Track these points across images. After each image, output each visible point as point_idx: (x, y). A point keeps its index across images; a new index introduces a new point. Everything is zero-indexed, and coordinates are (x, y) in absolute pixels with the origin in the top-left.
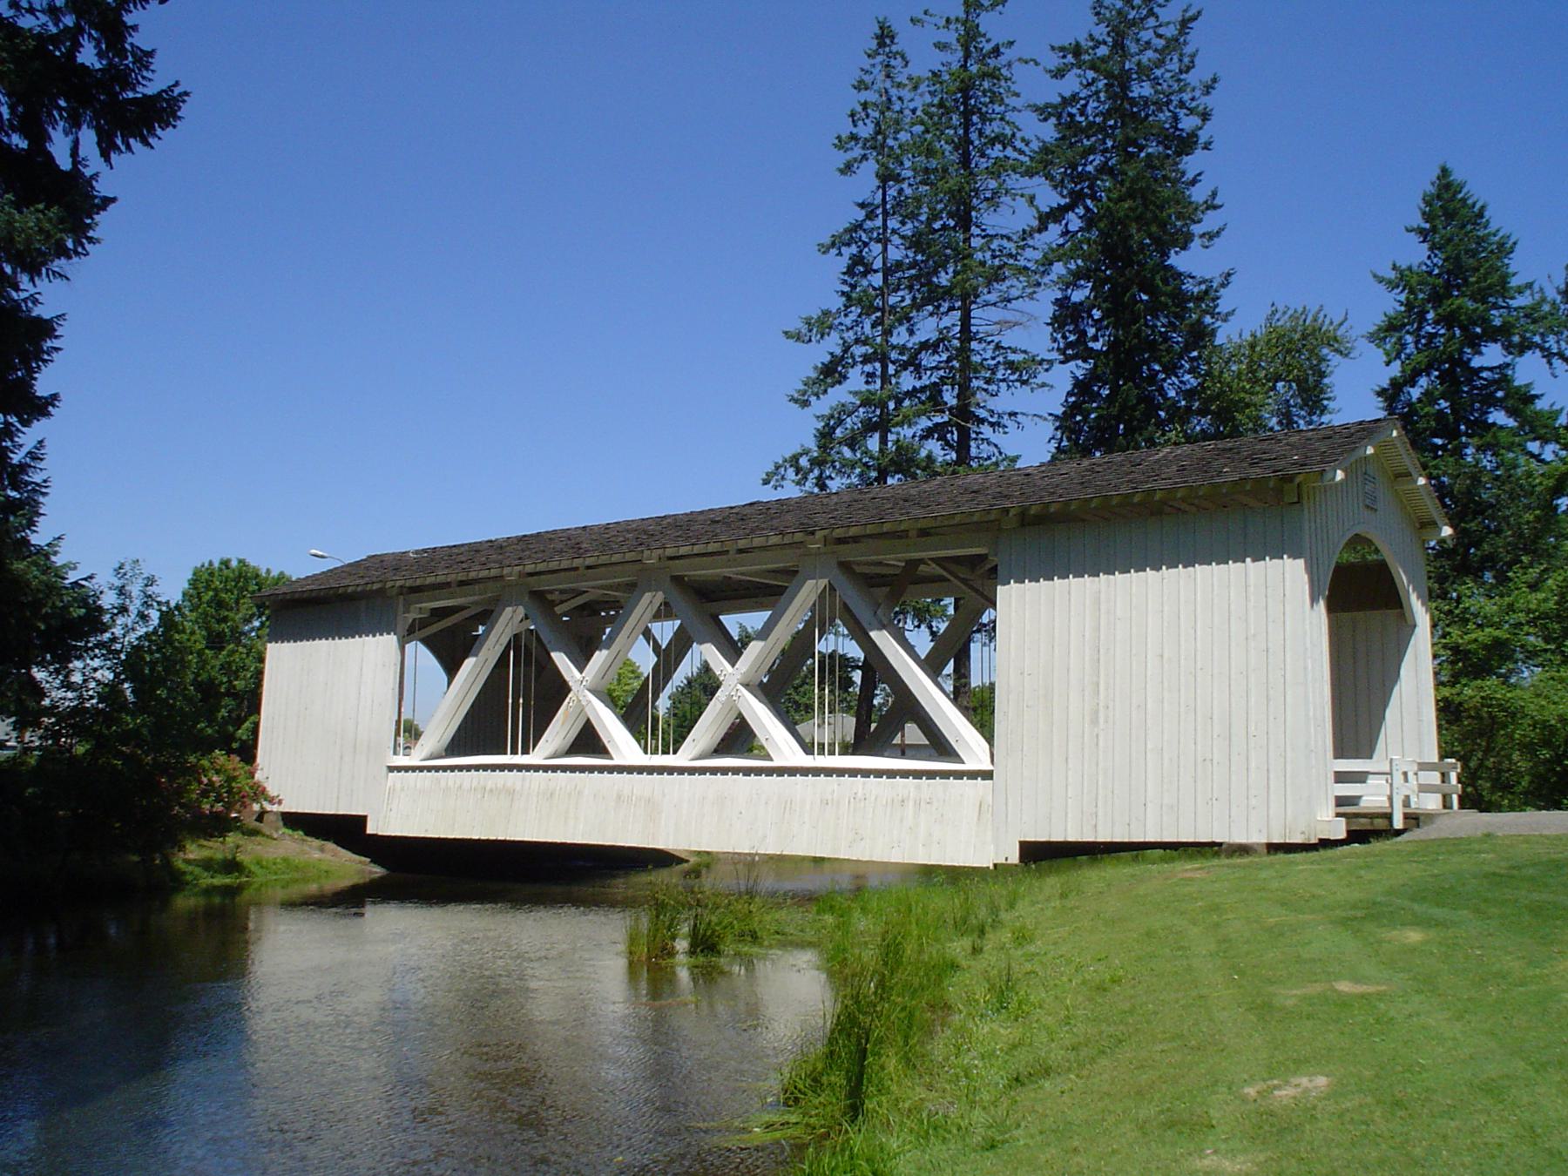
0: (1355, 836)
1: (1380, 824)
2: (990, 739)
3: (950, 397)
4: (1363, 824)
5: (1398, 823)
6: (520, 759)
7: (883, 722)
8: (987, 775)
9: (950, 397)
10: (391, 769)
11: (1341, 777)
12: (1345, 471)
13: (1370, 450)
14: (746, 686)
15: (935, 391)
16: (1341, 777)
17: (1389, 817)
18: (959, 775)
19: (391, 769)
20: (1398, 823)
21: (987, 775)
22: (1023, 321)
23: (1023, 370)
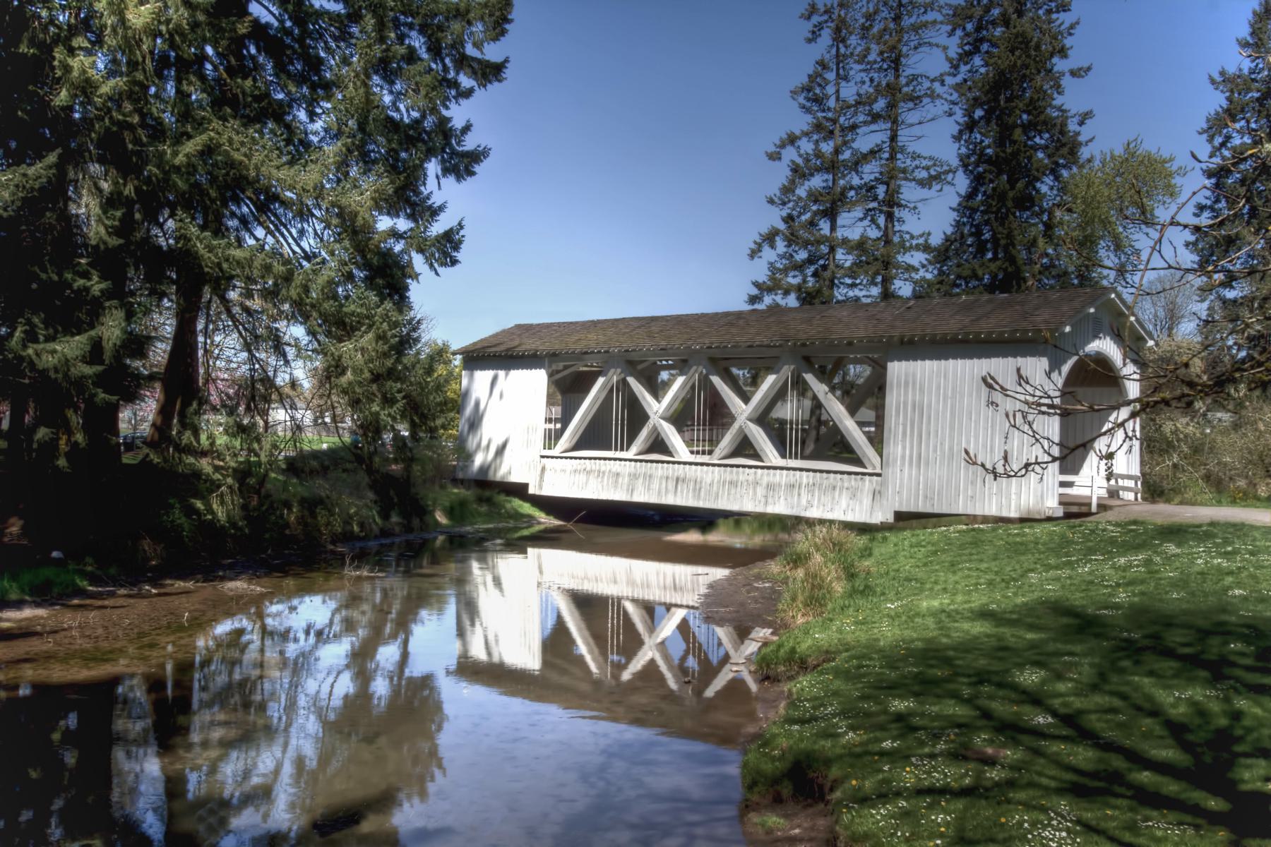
0: (1068, 516)
1: (1084, 509)
2: (881, 456)
3: (881, 191)
4: (1075, 509)
5: (1094, 509)
6: (619, 454)
7: (826, 445)
8: (879, 475)
9: (881, 191)
10: (543, 457)
11: (1063, 484)
12: (1072, 326)
13: (1092, 310)
14: (750, 420)
15: (871, 188)
16: (1063, 484)
17: (1089, 505)
18: (674, 463)
19: (543, 457)
20: (1094, 509)
21: (879, 475)
22: (936, 135)
23: (935, 179)
